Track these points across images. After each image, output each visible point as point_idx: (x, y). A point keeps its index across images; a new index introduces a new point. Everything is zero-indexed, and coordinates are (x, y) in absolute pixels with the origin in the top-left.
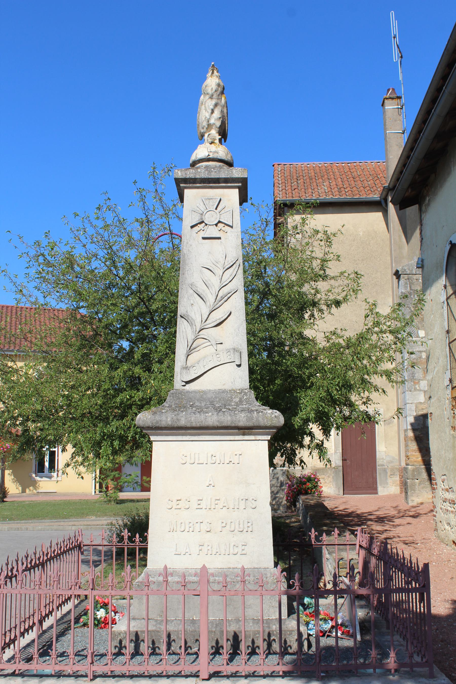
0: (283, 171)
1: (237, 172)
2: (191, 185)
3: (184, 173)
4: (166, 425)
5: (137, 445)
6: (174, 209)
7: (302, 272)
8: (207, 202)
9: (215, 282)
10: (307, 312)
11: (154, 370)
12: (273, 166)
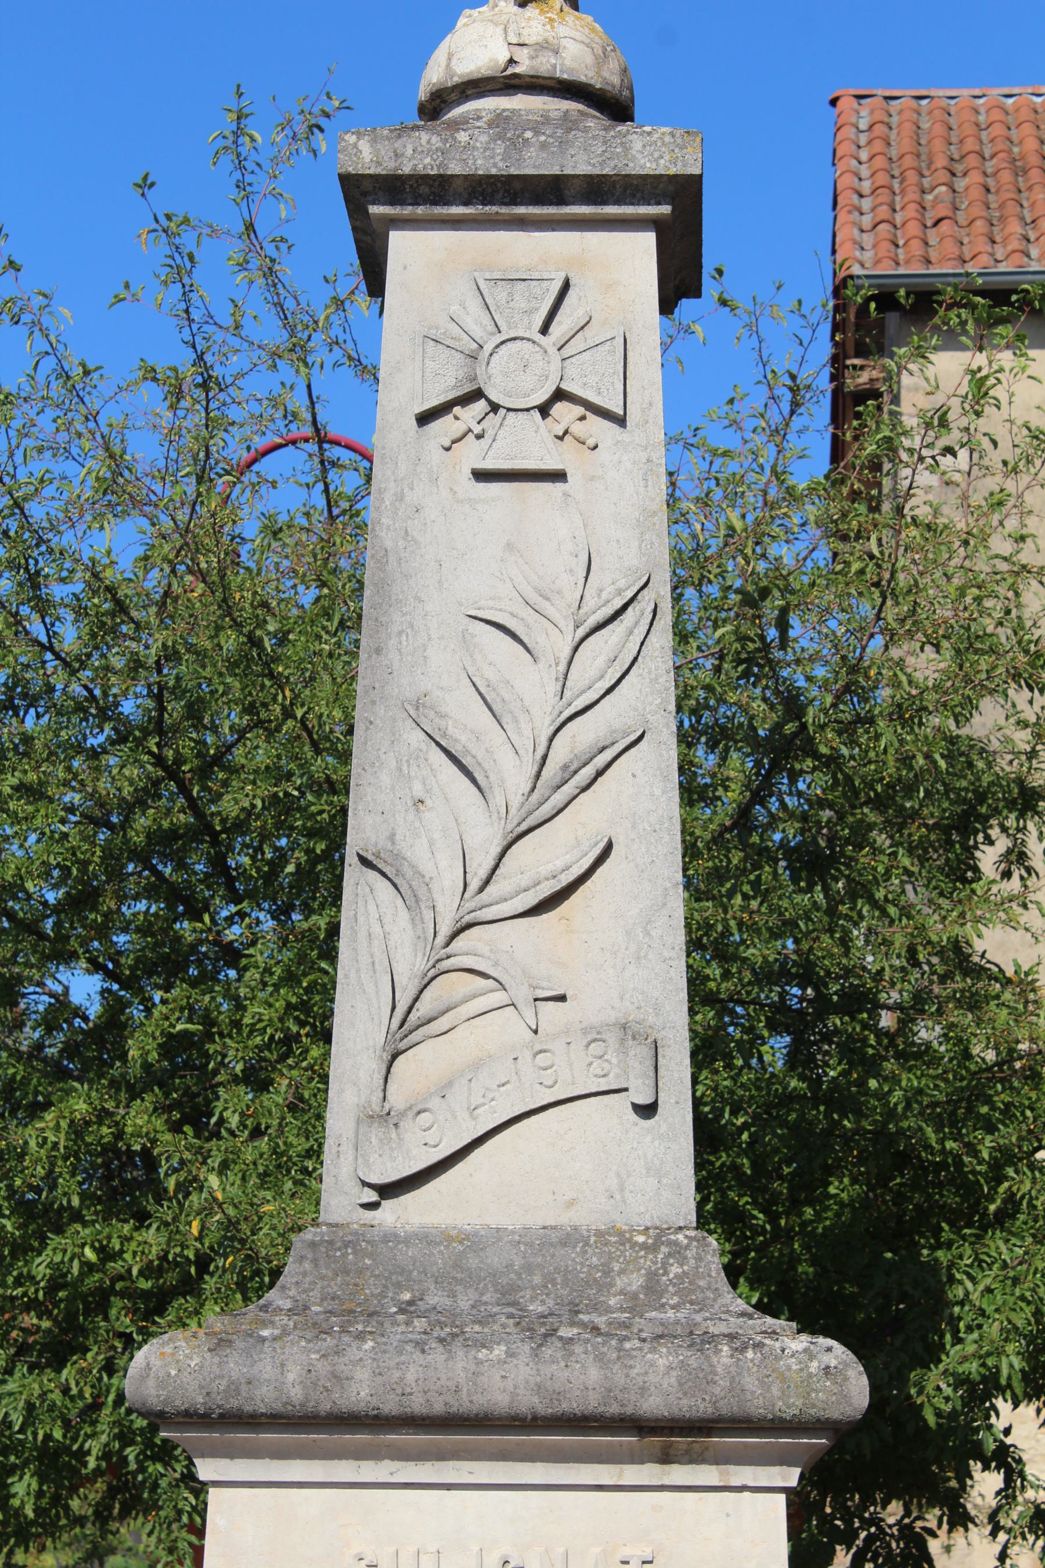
0: (880, 129)
1: (648, 149)
2: (420, 210)
3: (385, 150)
4: (278, 1407)
5: (128, 1496)
6: (337, 321)
7: (970, 644)
8: (498, 296)
9: (533, 690)
10: (991, 842)
11: (222, 1121)
12: (834, 102)
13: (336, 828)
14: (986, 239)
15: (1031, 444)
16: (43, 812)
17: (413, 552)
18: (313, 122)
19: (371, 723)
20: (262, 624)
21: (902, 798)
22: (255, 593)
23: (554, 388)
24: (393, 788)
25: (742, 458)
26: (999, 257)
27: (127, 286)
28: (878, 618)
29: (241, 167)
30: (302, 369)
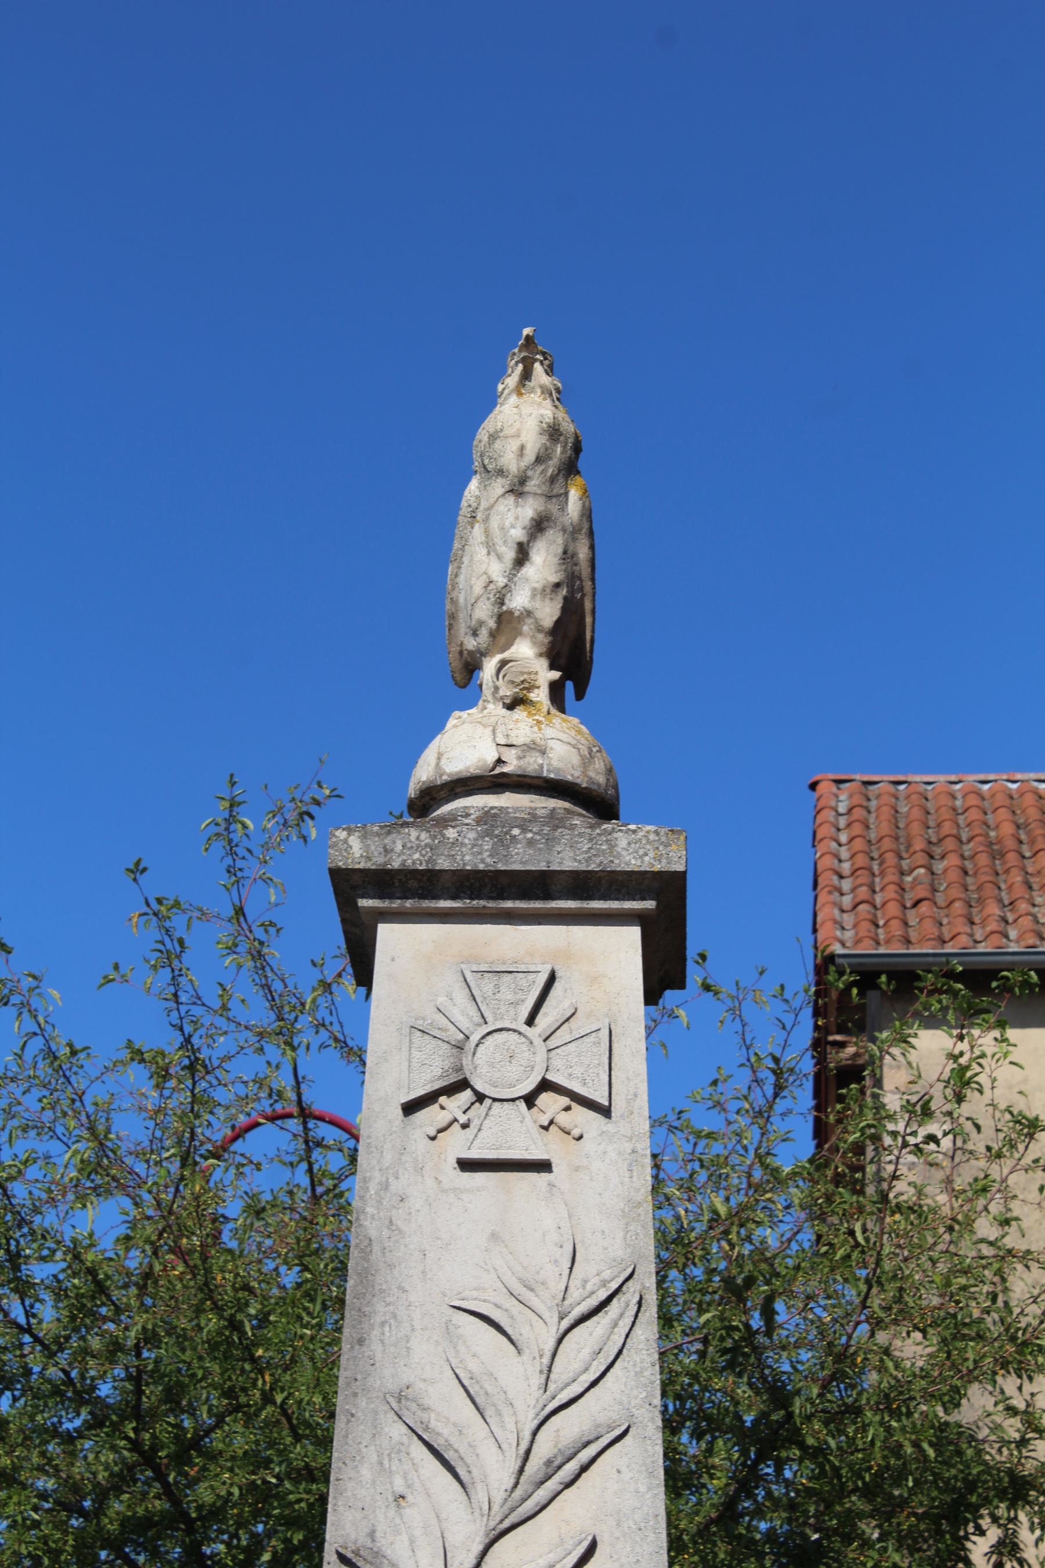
0: (858, 813)
1: (634, 847)
2: (408, 904)
3: (375, 845)
6: (323, 1002)
7: (955, 1331)
8: (484, 987)
9: (517, 1383)
10: (982, 1533)
12: (813, 786)
13: (313, 1517)
14: (966, 921)
15: (1014, 1128)
16: (15, 1499)
17: (397, 1242)
18: (304, 809)
19: (353, 1415)
20: (242, 1306)
21: (891, 1486)
22: (237, 1275)
23: (539, 1078)
24: (374, 1482)
25: (726, 1140)
26: (978, 937)
27: (116, 967)
28: (864, 1306)
29: (232, 853)
30: (289, 1052)
